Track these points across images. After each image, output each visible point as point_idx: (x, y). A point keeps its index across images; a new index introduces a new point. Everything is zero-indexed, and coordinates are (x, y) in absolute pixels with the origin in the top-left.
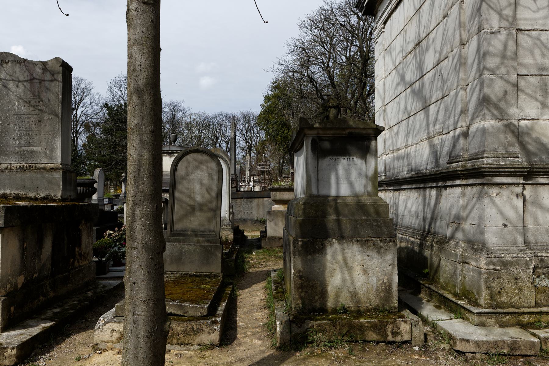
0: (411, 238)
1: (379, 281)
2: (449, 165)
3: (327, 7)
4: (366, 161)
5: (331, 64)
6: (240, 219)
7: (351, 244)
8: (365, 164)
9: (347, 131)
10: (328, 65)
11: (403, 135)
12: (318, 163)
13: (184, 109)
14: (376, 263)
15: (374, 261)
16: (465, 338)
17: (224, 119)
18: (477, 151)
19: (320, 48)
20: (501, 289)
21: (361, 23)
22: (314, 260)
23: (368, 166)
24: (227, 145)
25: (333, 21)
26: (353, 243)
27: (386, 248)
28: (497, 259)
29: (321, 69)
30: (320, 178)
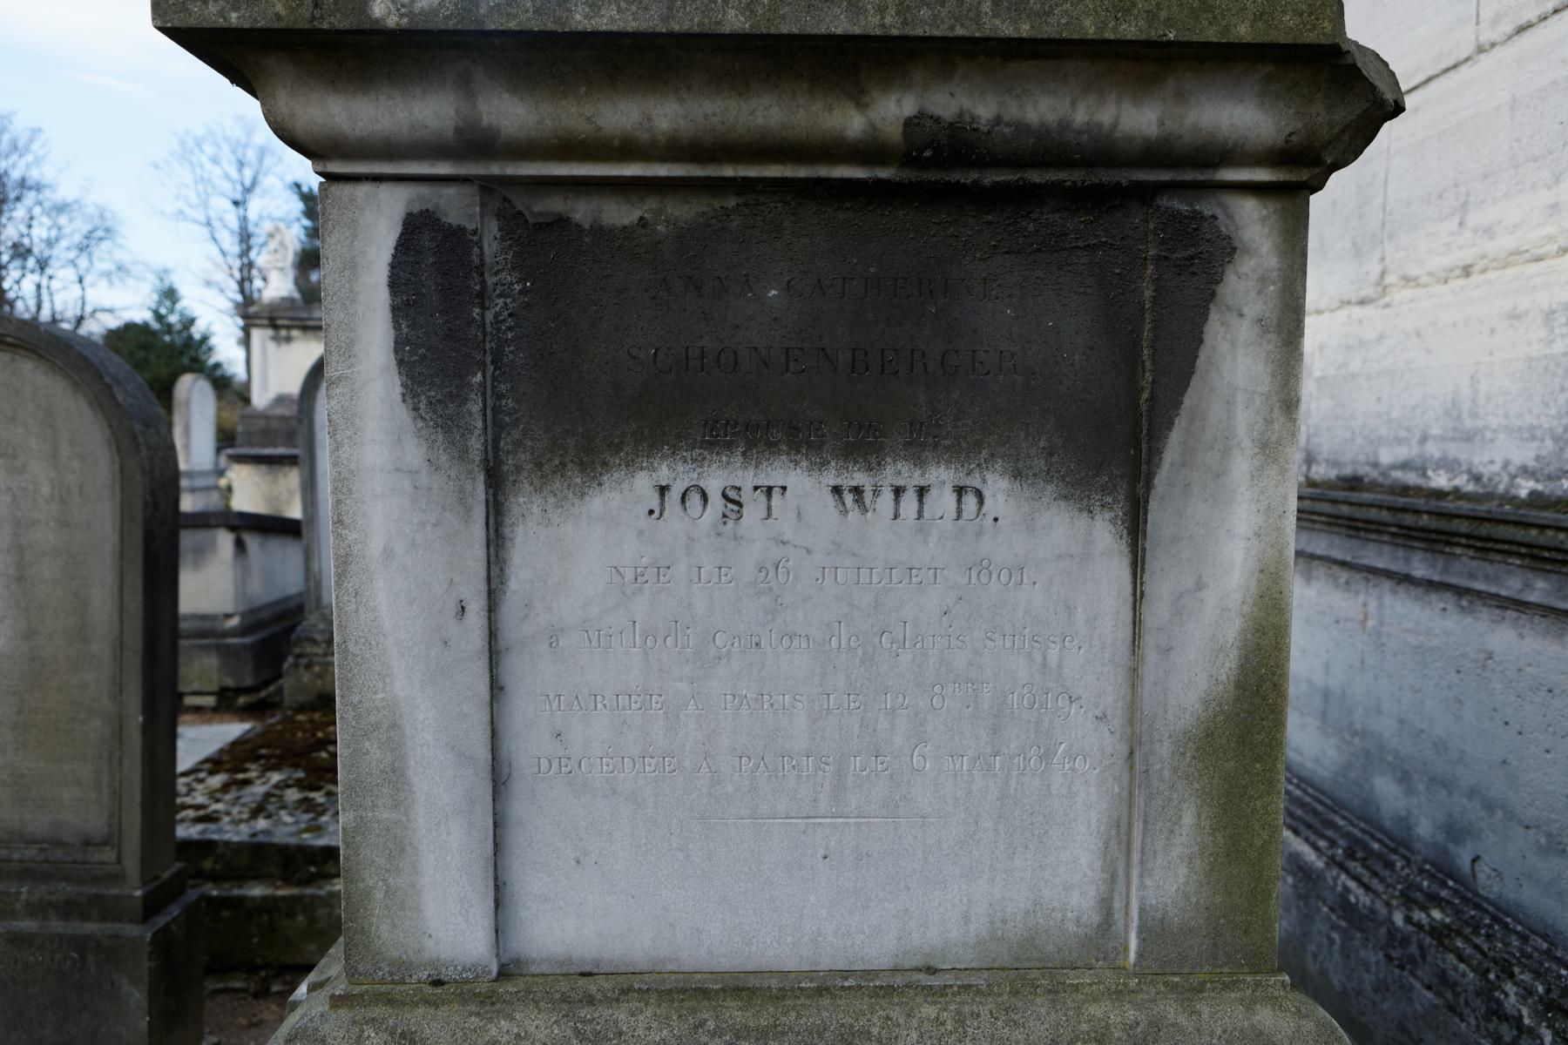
8: (1114, 569)
9: (890, 110)
12: (496, 541)
23: (1161, 588)
30: (529, 745)
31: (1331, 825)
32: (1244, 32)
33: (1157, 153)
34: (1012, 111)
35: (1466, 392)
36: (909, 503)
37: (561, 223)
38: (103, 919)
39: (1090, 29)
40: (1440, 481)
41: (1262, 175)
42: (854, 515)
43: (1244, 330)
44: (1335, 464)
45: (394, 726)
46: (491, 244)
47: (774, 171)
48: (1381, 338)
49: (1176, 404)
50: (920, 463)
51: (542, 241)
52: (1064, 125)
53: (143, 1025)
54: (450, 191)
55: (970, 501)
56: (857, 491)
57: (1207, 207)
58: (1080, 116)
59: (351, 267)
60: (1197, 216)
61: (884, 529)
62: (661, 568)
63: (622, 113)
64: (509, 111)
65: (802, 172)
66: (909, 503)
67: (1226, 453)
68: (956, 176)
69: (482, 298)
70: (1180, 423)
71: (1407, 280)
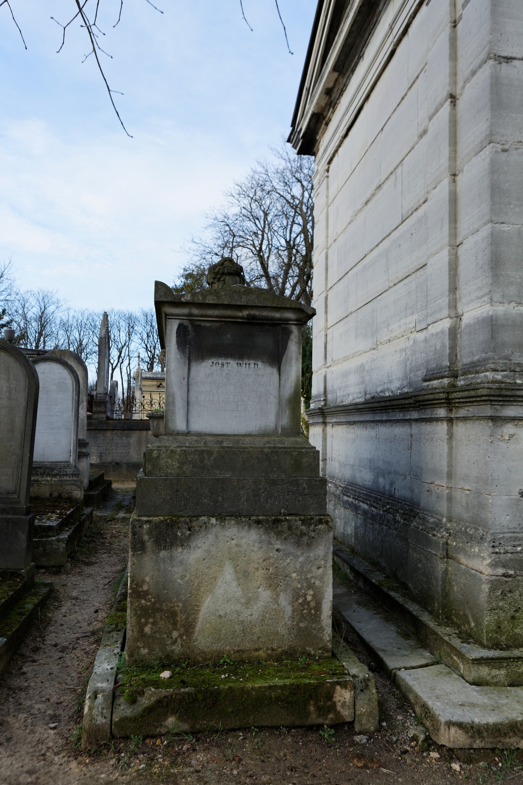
0: (361, 504)
1: (298, 599)
2: (426, 384)
3: (260, 169)
4: (279, 370)
5: (264, 247)
6: (110, 463)
7: (246, 527)
8: (277, 376)
9: (245, 313)
10: (261, 248)
11: (355, 347)
12: (189, 369)
13: (58, 301)
14: (292, 565)
15: (288, 561)
16: (455, 719)
17: (117, 317)
18: (476, 358)
19: (250, 225)
20: (516, 611)
21: (306, 194)
22: (171, 558)
23: (283, 378)
24: (121, 353)
25: (268, 188)
26: (250, 526)
27: (313, 534)
28: (510, 555)
29: (251, 254)
30: (192, 399)
31: (371, 497)
32: (288, 306)
33: (280, 319)
34: (261, 314)
35: (390, 371)
36: (247, 365)
37: (200, 325)
38: (14, 514)
39: (270, 305)
40: (387, 394)
41: (294, 323)
42: (240, 367)
43: (294, 343)
44: (370, 394)
45: (174, 395)
46: (190, 328)
47: (229, 320)
48: (377, 358)
49: (284, 353)
50: (249, 360)
51: (197, 328)
52: (268, 316)
53: (24, 546)
54: (185, 321)
55: (256, 366)
56: (240, 364)
57: (288, 326)
58: (270, 315)
59: (171, 330)
60: (287, 328)
61: (244, 369)
62: (212, 374)
63: (210, 312)
64: (195, 311)
65: (233, 320)
66: (247, 365)
67: (291, 360)
68: (253, 321)
69: (189, 335)
70: (285, 355)
71: (381, 343)
